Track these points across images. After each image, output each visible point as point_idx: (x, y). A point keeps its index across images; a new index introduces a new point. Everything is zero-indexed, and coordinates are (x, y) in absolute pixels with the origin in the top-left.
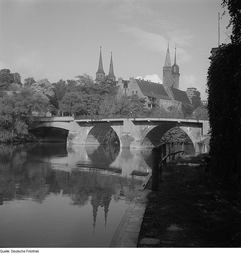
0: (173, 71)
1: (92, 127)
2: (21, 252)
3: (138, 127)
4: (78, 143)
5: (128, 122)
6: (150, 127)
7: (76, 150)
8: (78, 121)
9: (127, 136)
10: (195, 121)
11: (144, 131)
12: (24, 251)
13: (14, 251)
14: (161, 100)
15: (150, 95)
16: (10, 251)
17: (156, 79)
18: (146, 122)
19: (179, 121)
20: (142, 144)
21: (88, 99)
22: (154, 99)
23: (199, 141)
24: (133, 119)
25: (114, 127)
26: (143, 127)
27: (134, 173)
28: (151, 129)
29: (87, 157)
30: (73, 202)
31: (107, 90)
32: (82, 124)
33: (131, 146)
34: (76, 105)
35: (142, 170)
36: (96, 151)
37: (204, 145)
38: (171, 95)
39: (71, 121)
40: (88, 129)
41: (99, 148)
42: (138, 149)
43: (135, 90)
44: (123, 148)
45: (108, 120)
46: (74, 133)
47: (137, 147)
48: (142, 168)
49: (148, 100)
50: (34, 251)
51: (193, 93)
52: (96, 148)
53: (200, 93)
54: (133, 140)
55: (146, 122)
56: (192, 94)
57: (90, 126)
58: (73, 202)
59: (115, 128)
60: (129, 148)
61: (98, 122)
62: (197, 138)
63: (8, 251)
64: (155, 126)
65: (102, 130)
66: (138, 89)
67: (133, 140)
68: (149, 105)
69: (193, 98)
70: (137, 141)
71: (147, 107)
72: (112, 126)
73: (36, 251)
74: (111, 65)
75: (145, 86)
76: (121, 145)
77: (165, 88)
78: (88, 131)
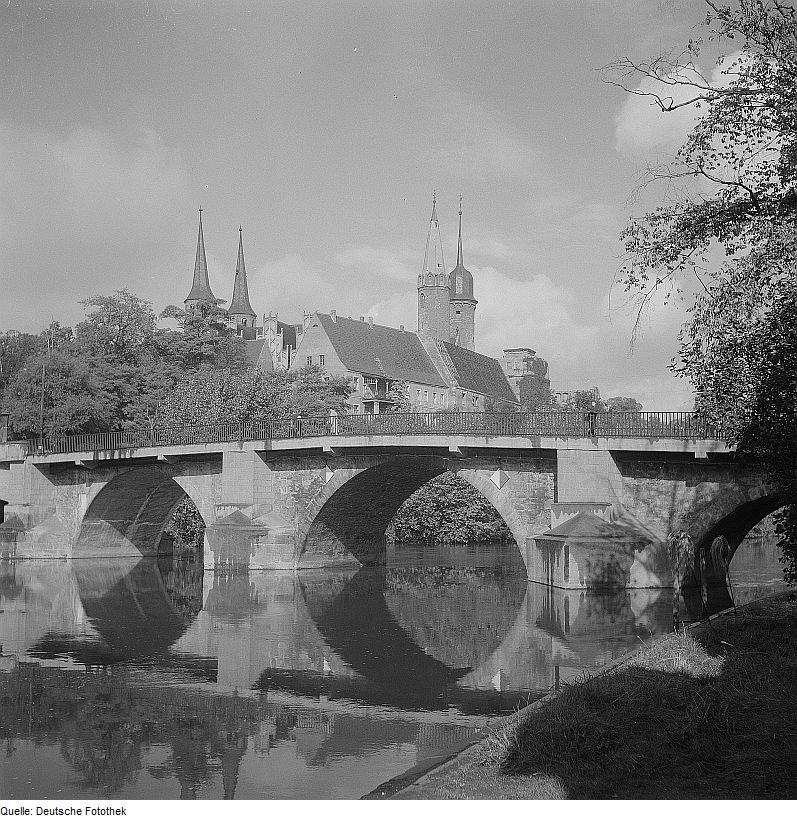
0: (451, 289)
1: (102, 485)
2: (68, 812)
3: (284, 480)
4: (42, 554)
5: (241, 457)
6: (335, 478)
7: (35, 586)
8: (42, 460)
9: (238, 518)
10: (523, 443)
11: (309, 494)
12: (79, 811)
13: (46, 812)
14: (411, 388)
15: (369, 370)
16: (34, 812)
17: (399, 312)
18: (315, 456)
19: (454, 443)
20: (304, 550)
21: (128, 381)
22: (383, 384)
23: (540, 531)
24: (261, 446)
25: (185, 482)
26: (307, 477)
27: (270, 680)
28: (337, 486)
29: (80, 612)
30: (80, 777)
31: (206, 349)
32: (59, 473)
33: (254, 563)
34: (71, 403)
35: (304, 662)
36: (122, 582)
37: (567, 548)
38: (444, 368)
39: (12, 462)
40: (85, 494)
41: (140, 573)
42: (286, 574)
43: (315, 353)
44: (215, 570)
45: (161, 453)
46: (26, 511)
47: (280, 564)
48: (304, 656)
49: (362, 390)
50: (109, 810)
51: (522, 365)
52: (125, 572)
53: (547, 364)
54: (260, 533)
55: (315, 456)
56: (521, 368)
57: (91, 481)
58: (80, 777)
59: (192, 485)
60: (244, 570)
61: (123, 462)
62: (533, 516)
63: (26, 812)
64: (355, 472)
65: (141, 494)
66: (328, 349)
67: (260, 533)
68: (369, 406)
69: (524, 382)
70: (282, 540)
71: (361, 410)
72: (178, 480)
73: (118, 811)
74: (241, 275)
75: (346, 334)
76: (209, 560)
77: (426, 344)
78: (84, 502)
